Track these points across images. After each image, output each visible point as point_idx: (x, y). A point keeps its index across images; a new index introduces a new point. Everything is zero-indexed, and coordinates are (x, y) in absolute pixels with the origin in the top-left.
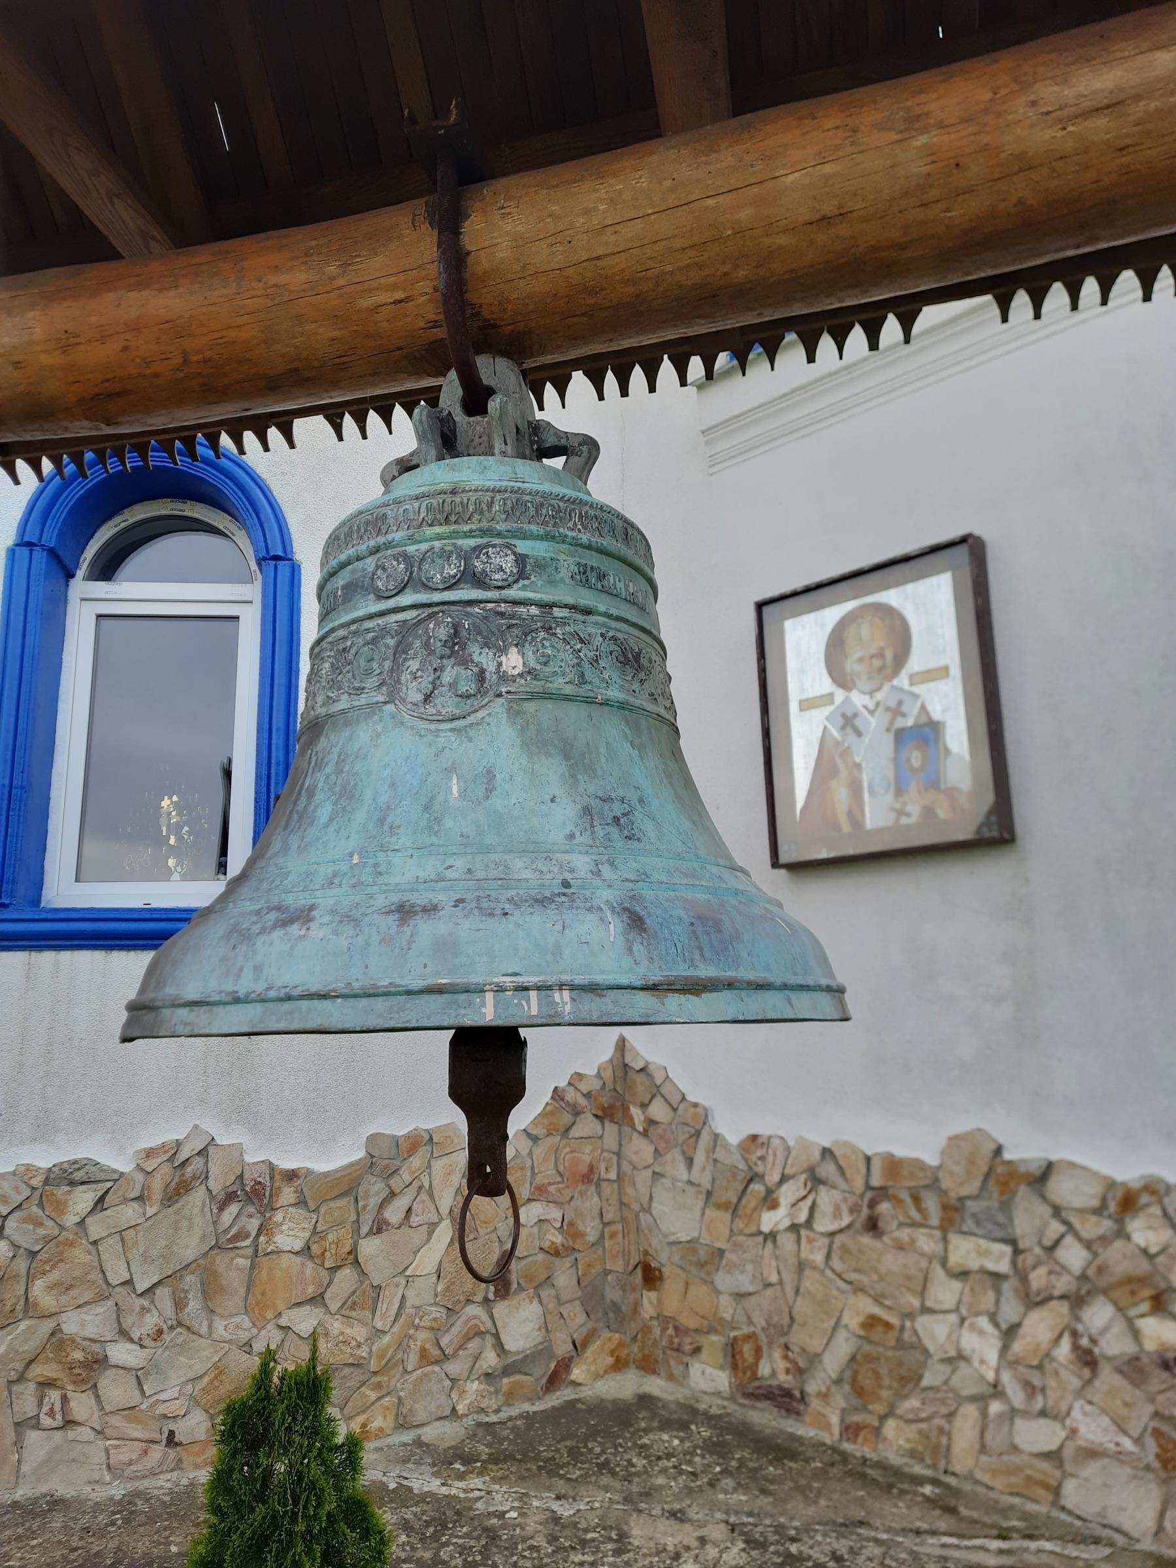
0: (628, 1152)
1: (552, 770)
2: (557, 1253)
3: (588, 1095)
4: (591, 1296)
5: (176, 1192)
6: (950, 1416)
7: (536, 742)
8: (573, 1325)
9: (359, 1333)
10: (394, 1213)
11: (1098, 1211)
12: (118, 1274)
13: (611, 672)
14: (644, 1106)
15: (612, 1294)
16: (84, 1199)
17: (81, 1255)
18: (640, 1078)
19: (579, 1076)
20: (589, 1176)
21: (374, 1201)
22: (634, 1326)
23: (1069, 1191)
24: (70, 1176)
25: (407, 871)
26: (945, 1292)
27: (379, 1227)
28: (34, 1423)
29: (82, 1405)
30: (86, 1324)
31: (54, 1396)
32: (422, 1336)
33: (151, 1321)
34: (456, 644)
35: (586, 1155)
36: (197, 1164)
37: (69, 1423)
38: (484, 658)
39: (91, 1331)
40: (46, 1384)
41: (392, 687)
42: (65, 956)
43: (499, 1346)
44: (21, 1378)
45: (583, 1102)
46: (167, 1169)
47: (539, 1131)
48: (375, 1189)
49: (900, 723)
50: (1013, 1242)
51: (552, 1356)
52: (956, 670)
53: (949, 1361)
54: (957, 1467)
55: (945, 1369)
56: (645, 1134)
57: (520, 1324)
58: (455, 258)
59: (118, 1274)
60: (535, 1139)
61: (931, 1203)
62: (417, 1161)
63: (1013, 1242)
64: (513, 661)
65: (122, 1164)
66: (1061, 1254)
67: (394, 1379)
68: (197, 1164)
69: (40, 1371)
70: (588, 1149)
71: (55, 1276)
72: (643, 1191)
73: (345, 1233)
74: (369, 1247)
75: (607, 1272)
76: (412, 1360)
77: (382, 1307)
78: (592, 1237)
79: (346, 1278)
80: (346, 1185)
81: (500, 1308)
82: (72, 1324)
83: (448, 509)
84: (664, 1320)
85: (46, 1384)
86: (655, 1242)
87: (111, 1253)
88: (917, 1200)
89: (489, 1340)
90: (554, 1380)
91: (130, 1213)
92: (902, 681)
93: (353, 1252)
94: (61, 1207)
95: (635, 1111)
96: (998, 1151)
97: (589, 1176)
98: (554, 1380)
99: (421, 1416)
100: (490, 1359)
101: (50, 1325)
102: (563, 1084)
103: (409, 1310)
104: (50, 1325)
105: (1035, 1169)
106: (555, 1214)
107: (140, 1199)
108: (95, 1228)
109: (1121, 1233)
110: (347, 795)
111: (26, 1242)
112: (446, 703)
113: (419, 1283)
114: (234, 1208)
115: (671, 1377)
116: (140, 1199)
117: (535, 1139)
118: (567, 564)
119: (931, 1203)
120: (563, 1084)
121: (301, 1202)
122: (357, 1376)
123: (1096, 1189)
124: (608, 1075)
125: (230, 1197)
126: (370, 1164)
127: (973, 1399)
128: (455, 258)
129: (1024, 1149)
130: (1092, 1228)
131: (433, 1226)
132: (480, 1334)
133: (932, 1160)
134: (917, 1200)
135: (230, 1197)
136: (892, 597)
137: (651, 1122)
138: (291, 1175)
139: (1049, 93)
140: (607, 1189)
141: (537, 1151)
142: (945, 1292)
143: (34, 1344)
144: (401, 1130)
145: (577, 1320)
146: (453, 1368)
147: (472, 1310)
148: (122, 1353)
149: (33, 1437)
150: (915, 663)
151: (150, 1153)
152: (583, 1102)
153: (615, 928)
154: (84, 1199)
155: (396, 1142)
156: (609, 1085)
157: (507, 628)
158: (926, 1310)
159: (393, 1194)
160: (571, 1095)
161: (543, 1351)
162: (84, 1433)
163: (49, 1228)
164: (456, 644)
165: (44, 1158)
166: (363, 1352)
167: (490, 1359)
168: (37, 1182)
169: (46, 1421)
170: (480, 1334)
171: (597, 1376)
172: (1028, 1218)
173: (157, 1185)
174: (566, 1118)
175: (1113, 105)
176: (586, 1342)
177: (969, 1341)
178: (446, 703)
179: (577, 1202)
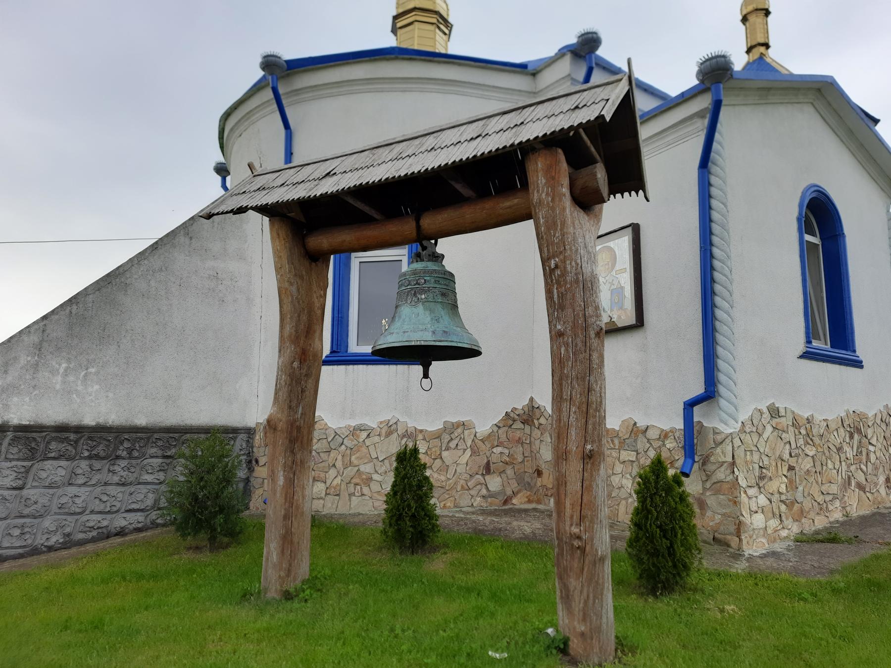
0: (533, 435)
1: (428, 313)
2: (507, 464)
3: (518, 415)
4: (519, 478)
5: (389, 434)
6: (618, 505)
7: (425, 309)
8: (513, 487)
9: (443, 478)
10: (453, 445)
11: (659, 439)
12: (374, 455)
13: (439, 296)
14: (538, 419)
15: (527, 479)
16: (364, 435)
17: (364, 450)
18: (537, 410)
19: (516, 409)
20: (519, 441)
21: (446, 441)
22: (535, 490)
23: (652, 434)
24: (360, 428)
25: (406, 327)
26: (619, 468)
27: (448, 449)
28: (354, 494)
29: (366, 490)
30: (367, 468)
31: (359, 487)
32: (462, 482)
33: (384, 468)
34: (415, 294)
35: (518, 434)
36: (394, 427)
37: (363, 495)
38: (419, 296)
39: (367, 471)
40: (356, 484)
41: (406, 300)
42: (356, 366)
43: (487, 488)
44: (350, 482)
45: (517, 417)
46: (386, 427)
47: (501, 425)
48: (446, 438)
49: (613, 287)
50: (637, 451)
51: (505, 495)
52: (628, 270)
53: (619, 488)
54: (620, 520)
55: (617, 491)
56: (538, 428)
57: (495, 483)
58: (418, 227)
59: (374, 455)
60: (499, 427)
61: (616, 441)
62: (460, 430)
63: (637, 451)
64: (423, 296)
65: (374, 426)
66: (648, 453)
67: (454, 492)
68: (394, 427)
69: (354, 481)
70: (518, 432)
71: (358, 455)
72: (538, 447)
73: (437, 449)
74: (445, 454)
75: (526, 472)
76: (459, 488)
77: (449, 472)
78: (520, 460)
79: (438, 462)
80: (438, 435)
81: (487, 477)
82: (362, 468)
83: (415, 272)
84: (543, 486)
85: (356, 484)
86: (541, 462)
87: (372, 448)
88: (612, 441)
89: (484, 486)
90: (506, 502)
91: (377, 439)
92: (614, 273)
93: (440, 454)
94: (358, 436)
95: (536, 421)
96: (635, 424)
97: (519, 441)
98: (506, 502)
99: (462, 505)
100: (484, 492)
101: (357, 468)
102: (509, 411)
103: (458, 474)
104: (357, 468)
105: (644, 428)
106: (506, 451)
107: (379, 435)
108: (368, 442)
109: (664, 445)
110: (400, 317)
111: (349, 445)
112: (413, 303)
113: (460, 466)
114: (405, 439)
115: (545, 504)
116: (379, 435)
117: (499, 427)
118: (433, 280)
119: (616, 441)
120: (509, 411)
121: (424, 439)
122: (443, 490)
123: (658, 433)
124: (526, 409)
125: (404, 436)
126: (445, 428)
127: (625, 499)
128: (418, 227)
129: (642, 423)
130: (656, 444)
131: (465, 450)
132: (481, 484)
133: (617, 428)
134: (612, 441)
135: (404, 436)
136: (611, 244)
137: (540, 424)
138: (421, 431)
139: (501, 205)
140: (526, 446)
141: (500, 431)
142: (619, 468)
143: (353, 474)
144: (454, 420)
145: (514, 485)
146: (473, 492)
147: (477, 476)
148: (376, 477)
149: (353, 498)
150: (617, 267)
151: (381, 423)
152: (517, 417)
153: (431, 334)
154: (364, 435)
155: (453, 424)
156: (527, 412)
157: (423, 291)
158: (613, 474)
159: (452, 439)
160: (512, 415)
161: (503, 492)
162: (367, 498)
163: (355, 442)
164: (415, 294)
165: (353, 423)
166: (444, 484)
167: (484, 492)
168: (351, 429)
169: (357, 494)
170: (481, 484)
171: (521, 503)
172: (641, 444)
173: (384, 432)
174: (511, 422)
175: (510, 207)
176: (518, 493)
177: (624, 481)
178: (413, 303)
179: (514, 448)
